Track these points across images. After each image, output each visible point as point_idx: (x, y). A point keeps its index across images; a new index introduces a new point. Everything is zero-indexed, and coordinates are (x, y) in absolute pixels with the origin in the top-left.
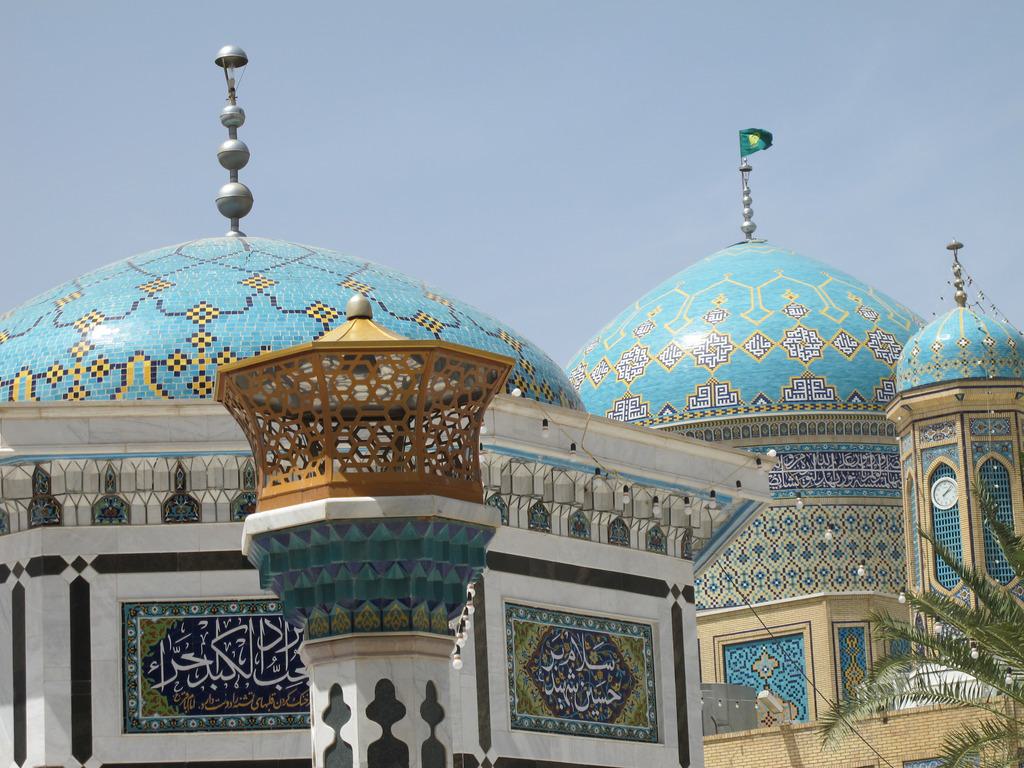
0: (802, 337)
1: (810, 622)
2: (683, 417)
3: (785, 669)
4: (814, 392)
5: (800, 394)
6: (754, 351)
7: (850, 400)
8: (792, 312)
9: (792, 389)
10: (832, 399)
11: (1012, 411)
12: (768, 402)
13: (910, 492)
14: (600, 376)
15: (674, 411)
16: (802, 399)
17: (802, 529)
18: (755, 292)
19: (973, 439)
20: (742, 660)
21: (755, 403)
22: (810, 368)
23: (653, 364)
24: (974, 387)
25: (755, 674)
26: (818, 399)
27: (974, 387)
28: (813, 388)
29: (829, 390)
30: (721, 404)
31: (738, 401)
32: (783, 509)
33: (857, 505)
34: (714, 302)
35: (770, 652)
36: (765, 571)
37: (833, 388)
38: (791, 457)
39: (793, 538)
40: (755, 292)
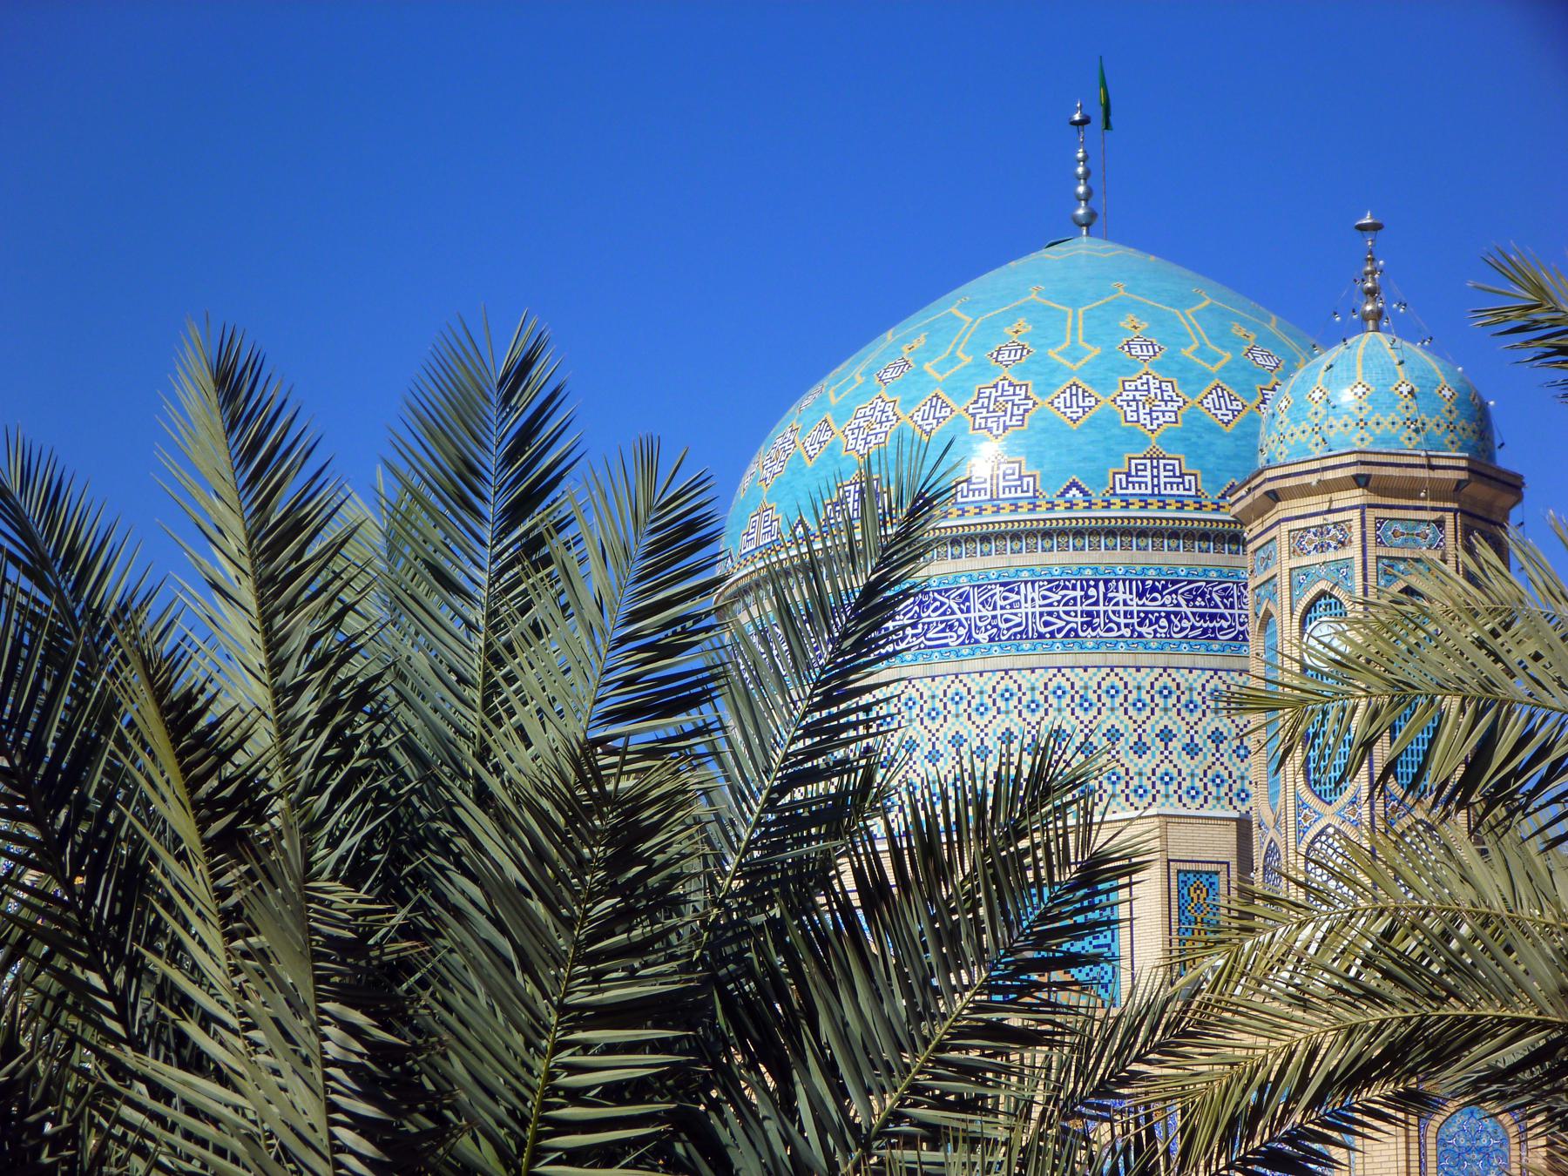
0: (1148, 390)
4: (1163, 480)
5: (1140, 483)
6: (1068, 410)
8: (1136, 351)
9: (1128, 475)
10: (1193, 492)
12: (1085, 493)
14: (817, 446)
16: (1143, 491)
17: (1055, 693)
18: (1075, 317)
19: (1382, 552)
21: (1062, 495)
23: (965, 430)
26: (1168, 492)
28: (1162, 474)
29: (1187, 478)
30: (1007, 495)
31: (1035, 491)
32: (1158, 671)
33: (1228, 671)
34: (1008, 331)
36: (1174, 772)
37: (1195, 475)
39: (1171, 721)
40: (1075, 317)
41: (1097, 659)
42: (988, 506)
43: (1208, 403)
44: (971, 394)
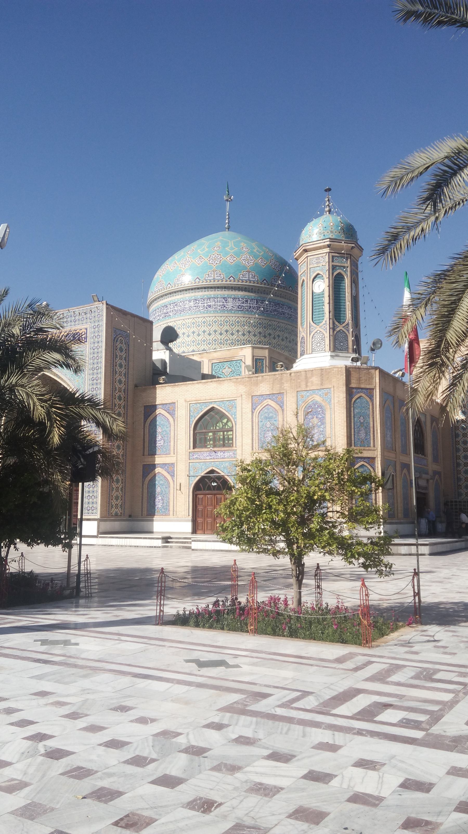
1: (245, 356)
2: (203, 282)
3: (234, 372)
7: (263, 281)
8: (244, 249)
11: (393, 487)
13: (302, 285)
15: (200, 280)
20: (219, 368)
21: (229, 278)
22: (250, 268)
24: (110, 639)
25: (223, 374)
27: (110, 639)
35: (229, 366)
38: (241, 299)
39: (195, 329)
41: (201, 316)
42: (212, 280)
43: (228, 259)
44: (208, 256)
